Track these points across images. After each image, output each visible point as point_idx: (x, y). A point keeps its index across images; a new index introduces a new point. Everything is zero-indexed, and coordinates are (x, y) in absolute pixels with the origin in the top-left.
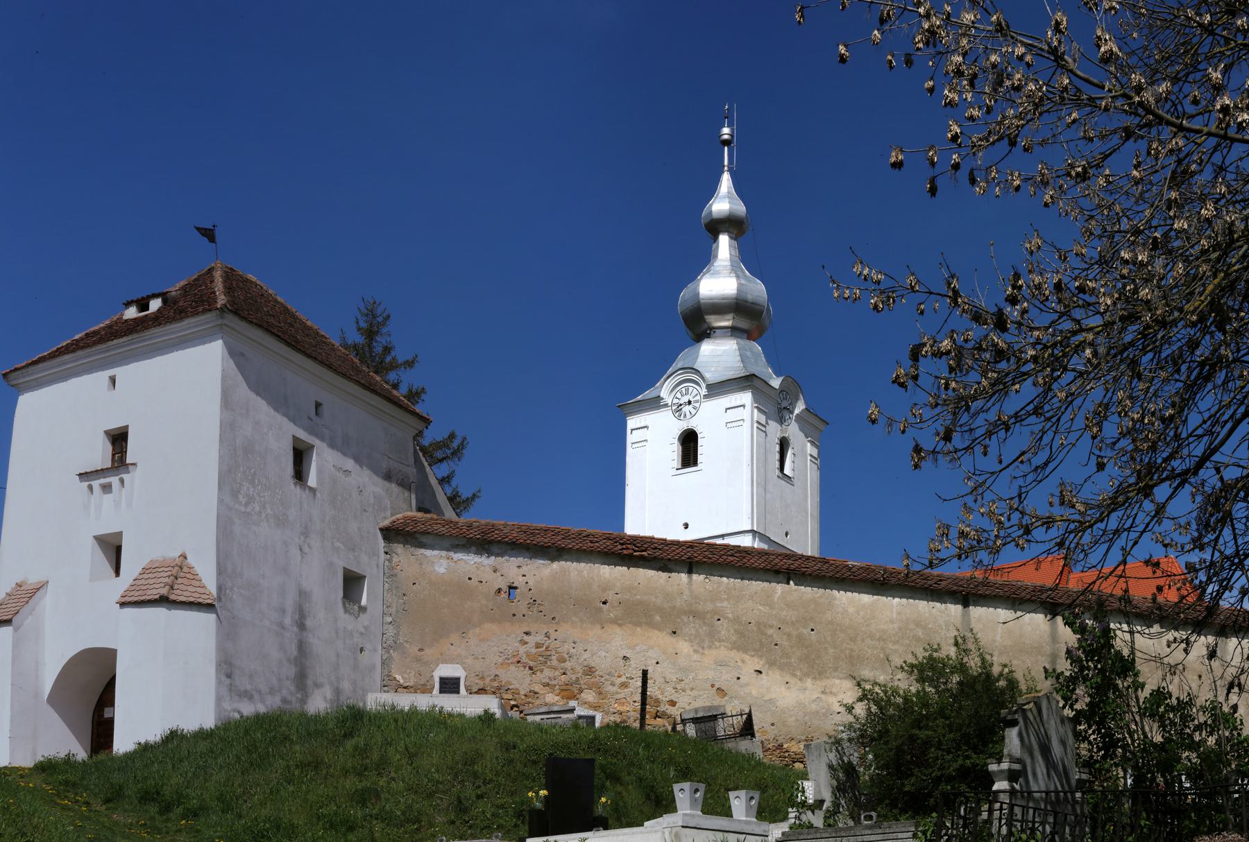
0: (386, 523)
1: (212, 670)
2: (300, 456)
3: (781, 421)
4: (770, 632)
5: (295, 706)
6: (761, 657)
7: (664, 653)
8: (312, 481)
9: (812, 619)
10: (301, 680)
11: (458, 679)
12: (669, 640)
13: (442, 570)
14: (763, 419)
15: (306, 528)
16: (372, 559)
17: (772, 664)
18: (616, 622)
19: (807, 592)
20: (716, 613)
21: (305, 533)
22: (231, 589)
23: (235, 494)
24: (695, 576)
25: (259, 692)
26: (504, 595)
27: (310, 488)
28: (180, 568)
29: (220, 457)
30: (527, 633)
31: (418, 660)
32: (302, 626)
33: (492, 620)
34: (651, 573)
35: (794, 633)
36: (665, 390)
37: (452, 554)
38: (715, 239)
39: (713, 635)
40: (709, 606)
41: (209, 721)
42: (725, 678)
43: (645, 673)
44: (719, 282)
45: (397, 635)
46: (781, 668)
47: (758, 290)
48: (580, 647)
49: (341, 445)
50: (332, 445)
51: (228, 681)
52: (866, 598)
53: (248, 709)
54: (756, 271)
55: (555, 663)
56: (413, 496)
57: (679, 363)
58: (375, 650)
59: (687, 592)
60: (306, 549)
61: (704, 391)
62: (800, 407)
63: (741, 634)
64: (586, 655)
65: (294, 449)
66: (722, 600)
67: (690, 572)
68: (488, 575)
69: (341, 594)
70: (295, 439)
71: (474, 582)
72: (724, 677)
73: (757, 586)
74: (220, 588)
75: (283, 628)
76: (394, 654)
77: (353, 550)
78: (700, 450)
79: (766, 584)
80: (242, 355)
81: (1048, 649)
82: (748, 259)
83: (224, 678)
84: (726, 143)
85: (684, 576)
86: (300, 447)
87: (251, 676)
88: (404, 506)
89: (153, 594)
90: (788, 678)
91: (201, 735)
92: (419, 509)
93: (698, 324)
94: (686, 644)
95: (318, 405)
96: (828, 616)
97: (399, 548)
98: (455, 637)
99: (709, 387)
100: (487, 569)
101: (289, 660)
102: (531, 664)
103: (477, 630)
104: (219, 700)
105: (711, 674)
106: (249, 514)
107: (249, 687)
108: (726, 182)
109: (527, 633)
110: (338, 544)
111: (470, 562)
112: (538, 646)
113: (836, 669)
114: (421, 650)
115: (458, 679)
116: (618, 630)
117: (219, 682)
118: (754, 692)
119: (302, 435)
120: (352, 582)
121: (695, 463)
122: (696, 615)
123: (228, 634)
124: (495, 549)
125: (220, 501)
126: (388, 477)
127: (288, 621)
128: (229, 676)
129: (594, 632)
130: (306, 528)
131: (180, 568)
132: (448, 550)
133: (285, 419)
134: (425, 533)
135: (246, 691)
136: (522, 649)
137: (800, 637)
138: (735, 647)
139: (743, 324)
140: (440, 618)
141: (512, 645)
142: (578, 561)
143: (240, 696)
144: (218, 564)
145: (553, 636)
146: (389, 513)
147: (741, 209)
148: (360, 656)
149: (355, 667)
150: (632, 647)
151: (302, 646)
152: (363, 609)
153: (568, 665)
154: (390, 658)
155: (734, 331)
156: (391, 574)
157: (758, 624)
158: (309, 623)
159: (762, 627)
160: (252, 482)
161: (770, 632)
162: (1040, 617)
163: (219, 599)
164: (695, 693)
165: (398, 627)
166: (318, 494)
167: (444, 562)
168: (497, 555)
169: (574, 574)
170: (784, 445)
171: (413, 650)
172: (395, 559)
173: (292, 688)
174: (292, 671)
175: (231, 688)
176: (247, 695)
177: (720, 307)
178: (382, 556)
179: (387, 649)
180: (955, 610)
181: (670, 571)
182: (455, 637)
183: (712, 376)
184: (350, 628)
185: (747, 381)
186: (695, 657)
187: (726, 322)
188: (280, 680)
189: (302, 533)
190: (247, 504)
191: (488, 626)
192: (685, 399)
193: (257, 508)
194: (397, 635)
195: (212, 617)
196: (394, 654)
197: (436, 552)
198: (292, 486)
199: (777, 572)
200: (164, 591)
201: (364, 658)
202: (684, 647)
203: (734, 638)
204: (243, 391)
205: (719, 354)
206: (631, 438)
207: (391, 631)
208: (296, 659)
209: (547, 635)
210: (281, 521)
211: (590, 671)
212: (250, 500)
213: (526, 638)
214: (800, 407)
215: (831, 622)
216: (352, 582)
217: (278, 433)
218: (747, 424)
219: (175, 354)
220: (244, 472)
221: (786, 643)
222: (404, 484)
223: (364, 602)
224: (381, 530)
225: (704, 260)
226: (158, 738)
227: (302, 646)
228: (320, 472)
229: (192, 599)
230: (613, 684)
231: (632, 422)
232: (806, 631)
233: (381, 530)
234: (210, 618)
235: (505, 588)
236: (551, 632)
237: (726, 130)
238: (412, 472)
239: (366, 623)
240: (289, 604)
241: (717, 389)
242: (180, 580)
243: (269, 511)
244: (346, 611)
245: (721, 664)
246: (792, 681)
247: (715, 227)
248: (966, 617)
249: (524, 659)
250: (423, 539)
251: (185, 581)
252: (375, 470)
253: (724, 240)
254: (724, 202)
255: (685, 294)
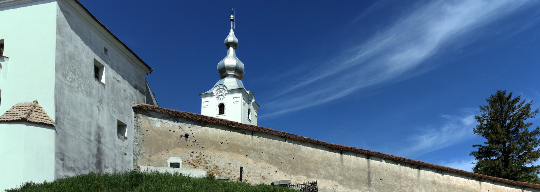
0: (135, 105)
1: (53, 156)
2: (98, 71)
3: (249, 104)
4: (280, 158)
5: (96, 171)
6: (277, 166)
7: (243, 163)
8: (103, 80)
9: (293, 154)
10: (99, 164)
11: (179, 164)
12: (245, 158)
13: (159, 126)
14: (244, 102)
15: (101, 99)
16: (129, 119)
17: (280, 169)
18: (225, 150)
19: (292, 145)
20: (261, 150)
21: (101, 102)
22: (63, 120)
23: (65, 76)
24: (254, 136)
25: (79, 168)
26: (184, 138)
27: (102, 83)
28: (34, 107)
29: (57, 56)
30: (192, 152)
31: (149, 160)
32: (99, 142)
33: (179, 147)
34: (238, 134)
35: (288, 159)
36: (214, 91)
37: (162, 120)
38: (228, 48)
39: (260, 157)
40: (259, 148)
41: (51, 178)
42: (265, 173)
43: (241, 169)
44: (231, 60)
45: (140, 150)
46: (284, 171)
47: (242, 65)
48: (213, 159)
49: (118, 70)
50: (112, 67)
51: (62, 162)
52: (311, 149)
53: (72, 174)
54: (241, 59)
55: (203, 164)
56: (145, 97)
57: (218, 83)
58: (131, 155)
59: (251, 142)
60: (101, 108)
61: (227, 92)
62: (253, 101)
63: (270, 158)
64: (215, 162)
65: (95, 66)
66: (263, 146)
67: (252, 135)
68: (177, 130)
69: (116, 130)
70: (95, 61)
71: (172, 132)
72: (265, 172)
73: (275, 142)
74: (57, 118)
75: (90, 141)
76: (139, 157)
77: (122, 114)
78: (225, 110)
79: (278, 141)
80: (68, 13)
81: (367, 170)
82: (239, 55)
83: (59, 161)
84: (232, 20)
85: (250, 136)
86: (98, 66)
87: (74, 161)
88: (142, 101)
89: (18, 117)
90: (286, 174)
91: (46, 186)
92: (147, 103)
93: (223, 73)
94: (251, 160)
95: (106, 50)
96: (299, 154)
97: (141, 116)
98: (164, 152)
99: (228, 91)
100: (177, 127)
101: (93, 155)
102: (194, 164)
103: (173, 150)
104: (57, 170)
105: (260, 171)
106: (72, 87)
107: (73, 166)
108: (232, 32)
109: (192, 152)
110: (115, 110)
111: (170, 124)
112: (197, 157)
113: (301, 172)
114: (150, 156)
115: (179, 164)
116: (226, 153)
117: (57, 162)
118: (275, 179)
119: (99, 59)
120: (121, 127)
121: (223, 113)
122: (255, 150)
123: (61, 140)
124: (180, 120)
125: (57, 77)
126: (136, 87)
127: (92, 138)
128: (62, 160)
129: (218, 153)
130: (101, 99)
131: (34, 107)
132: (161, 118)
133: (90, 50)
134: (152, 111)
135: (71, 168)
136: (191, 158)
137: (290, 161)
138: (268, 162)
139: (237, 75)
140: (160, 145)
141: (187, 157)
142: (212, 127)
143: (68, 169)
144: (56, 106)
145: (203, 154)
146: (136, 102)
147: (236, 40)
148: (124, 157)
149: (123, 161)
150: (232, 160)
151: (99, 150)
152: (126, 138)
153: (208, 165)
154: (137, 159)
155: (234, 76)
156: (137, 126)
157: (276, 155)
158: (102, 140)
159: (277, 156)
160: (74, 73)
161: (280, 158)
162: (365, 159)
163: (57, 123)
164: (254, 177)
165: (140, 147)
166: (106, 87)
167: (160, 123)
168: (181, 122)
169: (210, 132)
170: (249, 110)
171: (147, 156)
172: (139, 120)
173: (95, 168)
174: (95, 160)
175: (63, 165)
176: (72, 169)
177: (230, 69)
178: (134, 118)
179: (135, 155)
180: (338, 155)
181: (245, 134)
182: (164, 152)
183: (229, 87)
184: (120, 145)
185: (240, 90)
186: (254, 165)
187: (232, 73)
188: (89, 164)
189: (99, 102)
190: (71, 82)
191: (177, 148)
192: (221, 94)
193: (77, 85)
194: (140, 150)
195: (53, 131)
196: (139, 157)
197: (156, 119)
198: (94, 80)
199: (282, 137)
200: (25, 116)
201: (127, 158)
202: (250, 161)
203: (268, 159)
204: (68, 30)
205: (231, 82)
206: (203, 105)
207: (137, 148)
208: (96, 155)
209: (200, 154)
210: (89, 94)
211: (216, 168)
212: (73, 81)
213: (192, 154)
214: (253, 101)
215: (300, 156)
216: (121, 127)
217: (88, 57)
218: (240, 102)
219: (30, 7)
220: (70, 67)
221: (285, 162)
222: (141, 91)
223: (126, 135)
224: (133, 108)
225: (225, 54)
226: (19, 187)
227: (99, 150)
228: (107, 78)
229: (40, 121)
230: (225, 173)
231: (203, 100)
232: (292, 159)
233: (133, 108)
234: (52, 132)
235: (184, 135)
236: (202, 153)
237: (232, 16)
238: (145, 88)
239: (127, 144)
240: (93, 130)
241: (231, 91)
242: (34, 113)
243: (83, 88)
244: (119, 138)
245: (263, 168)
246: (287, 175)
247: (229, 45)
248: (342, 158)
249: (192, 162)
250: (151, 113)
251: (37, 113)
252: (130, 82)
253: (231, 49)
254: (231, 37)
255: (220, 64)
